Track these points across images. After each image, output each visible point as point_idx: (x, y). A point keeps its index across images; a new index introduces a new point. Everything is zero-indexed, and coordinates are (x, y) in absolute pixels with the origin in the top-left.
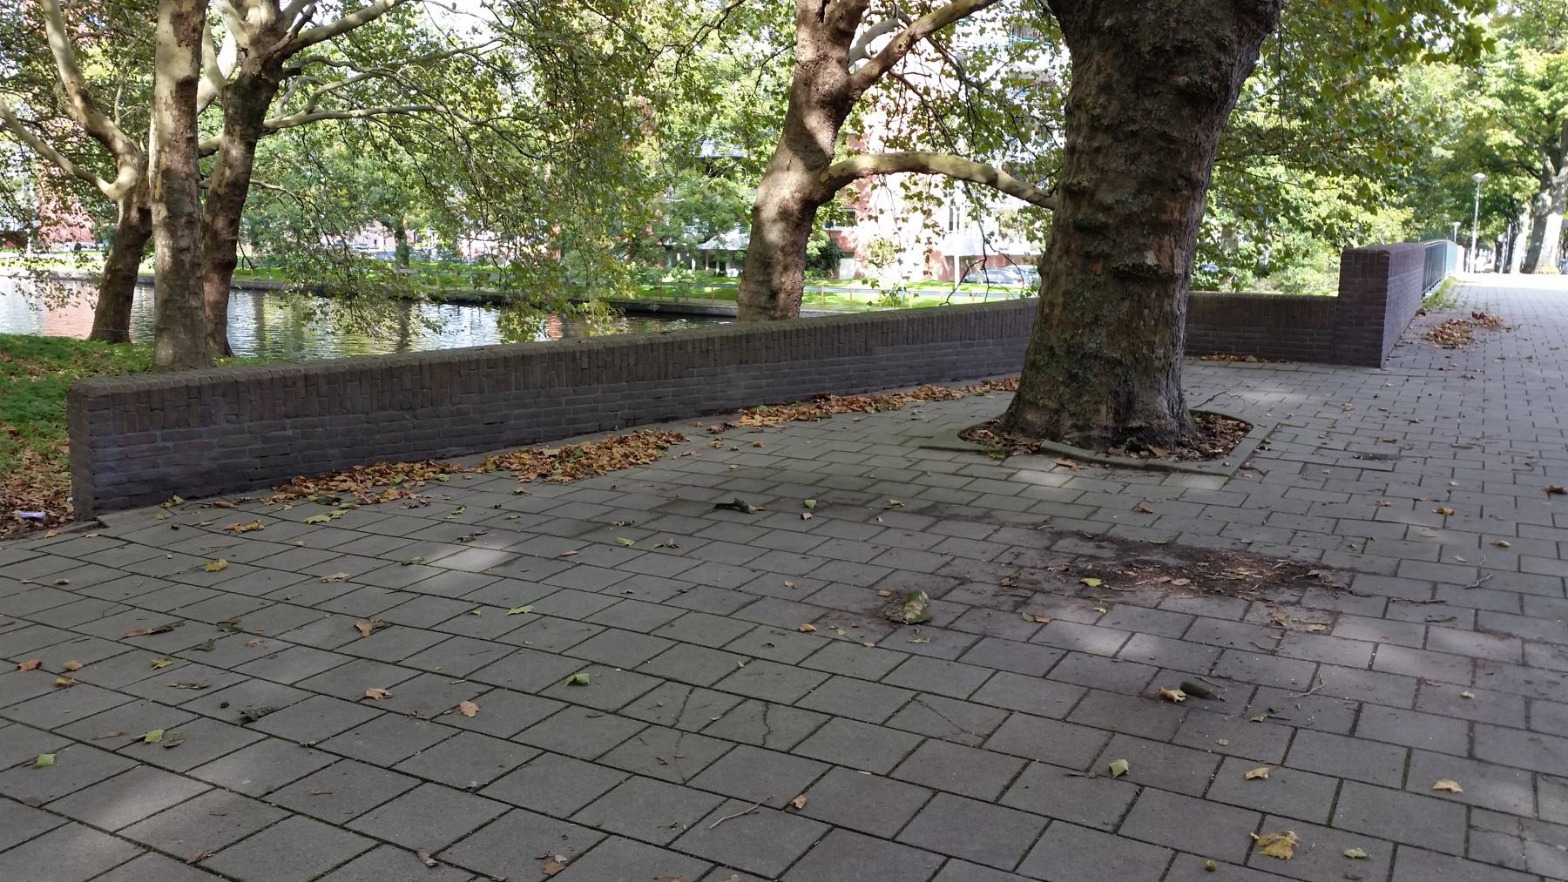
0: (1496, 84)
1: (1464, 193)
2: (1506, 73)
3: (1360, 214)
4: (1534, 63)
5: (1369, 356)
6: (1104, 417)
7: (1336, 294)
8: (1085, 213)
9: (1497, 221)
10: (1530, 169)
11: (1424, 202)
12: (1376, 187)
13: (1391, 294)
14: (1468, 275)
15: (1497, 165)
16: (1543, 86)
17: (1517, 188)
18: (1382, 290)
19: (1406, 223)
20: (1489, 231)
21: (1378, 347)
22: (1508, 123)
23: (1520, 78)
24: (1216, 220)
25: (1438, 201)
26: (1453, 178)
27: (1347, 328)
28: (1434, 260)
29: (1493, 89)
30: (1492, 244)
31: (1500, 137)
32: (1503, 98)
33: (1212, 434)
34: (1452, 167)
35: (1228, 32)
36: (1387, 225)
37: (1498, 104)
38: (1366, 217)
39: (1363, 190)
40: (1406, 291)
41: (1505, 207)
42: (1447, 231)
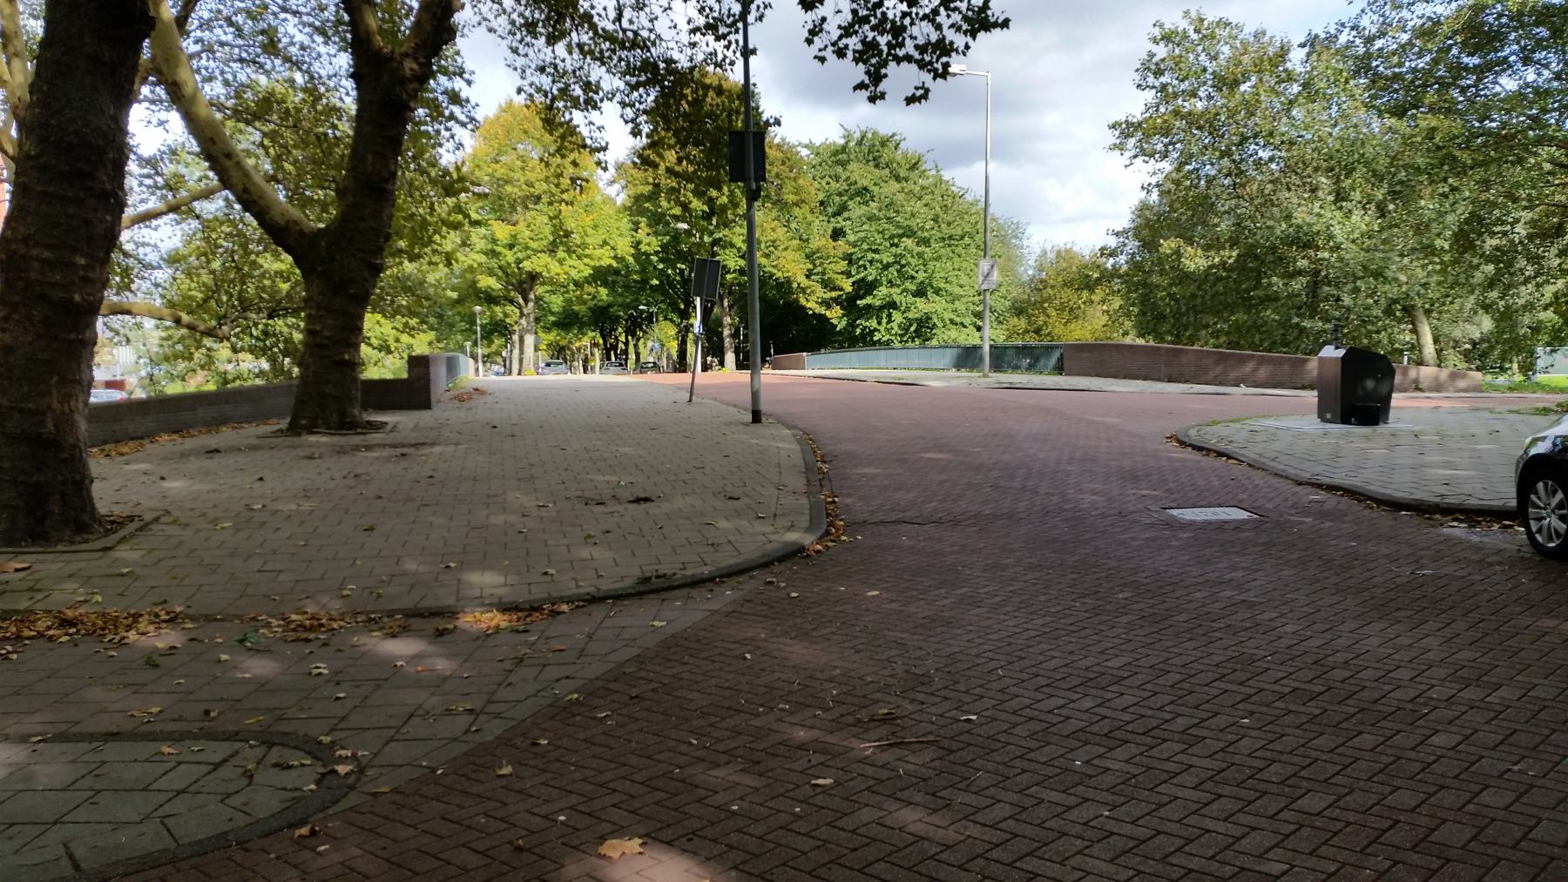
0: (480, 244)
1: (471, 319)
2: (485, 237)
3: (405, 338)
4: (502, 231)
5: (425, 404)
6: (335, 419)
7: (405, 376)
8: (318, 340)
9: (498, 342)
10: (512, 302)
11: (444, 327)
12: (413, 322)
13: (432, 375)
14: (472, 373)
15: (490, 299)
16: (511, 247)
17: (506, 315)
18: (428, 374)
19: (430, 344)
20: (494, 348)
21: (429, 400)
22: (491, 273)
23: (494, 241)
24: (298, 337)
25: (452, 326)
26: (460, 309)
27: (414, 389)
28: (452, 366)
29: (478, 247)
30: (499, 360)
31: (488, 282)
32: (486, 254)
33: (377, 427)
34: (458, 302)
35: (366, 274)
36: (422, 344)
37: (483, 259)
38: (411, 341)
39: (406, 325)
40: (439, 373)
41: (499, 329)
42: (462, 349)
